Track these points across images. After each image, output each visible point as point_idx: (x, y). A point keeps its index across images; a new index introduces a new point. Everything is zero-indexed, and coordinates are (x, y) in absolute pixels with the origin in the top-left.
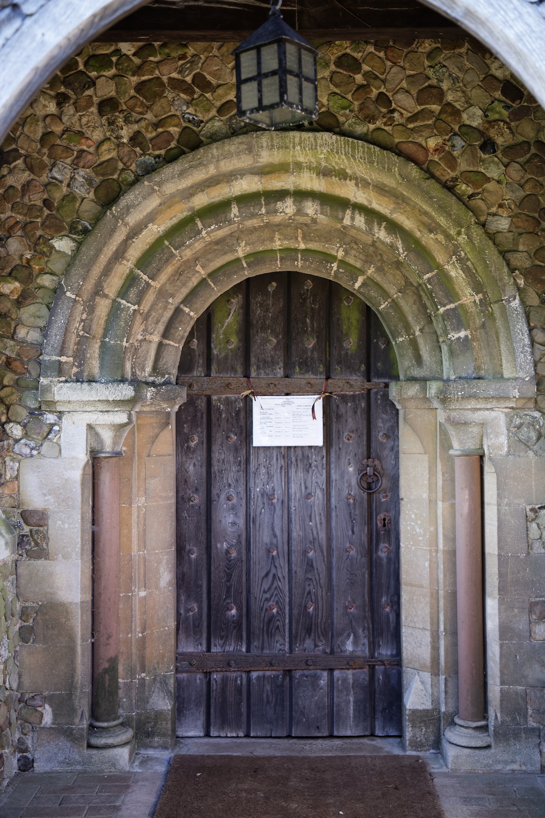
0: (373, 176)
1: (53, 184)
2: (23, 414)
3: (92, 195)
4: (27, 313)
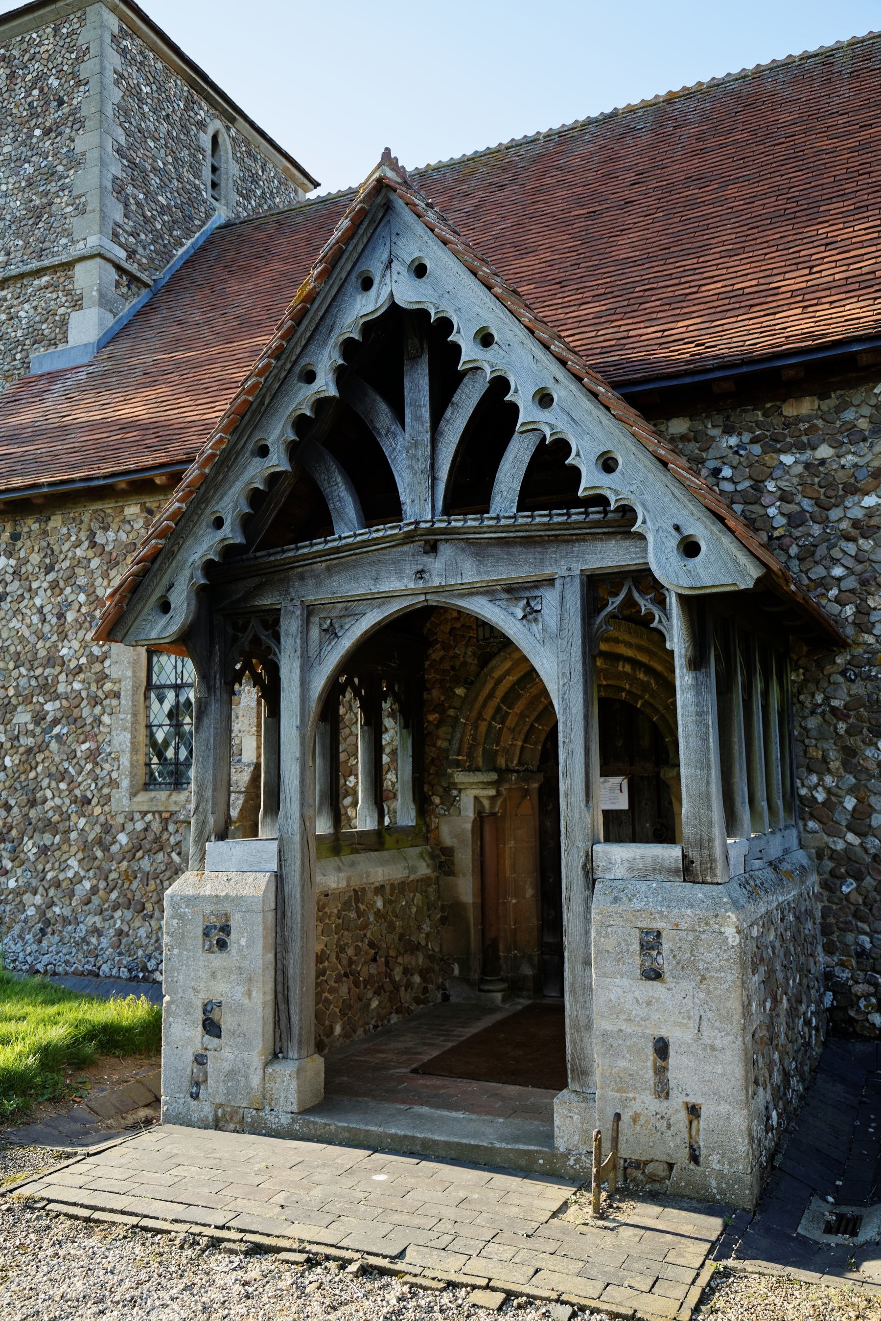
0: (634, 640)
1: (456, 656)
2: (440, 790)
3: (476, 662)
4: (443, 731)
